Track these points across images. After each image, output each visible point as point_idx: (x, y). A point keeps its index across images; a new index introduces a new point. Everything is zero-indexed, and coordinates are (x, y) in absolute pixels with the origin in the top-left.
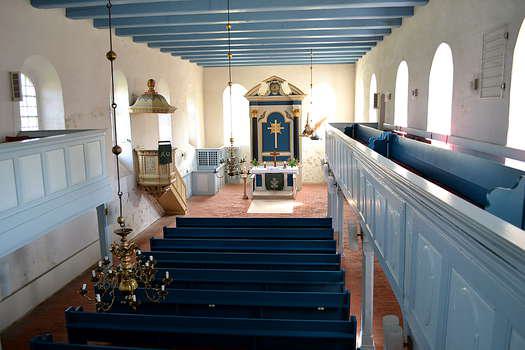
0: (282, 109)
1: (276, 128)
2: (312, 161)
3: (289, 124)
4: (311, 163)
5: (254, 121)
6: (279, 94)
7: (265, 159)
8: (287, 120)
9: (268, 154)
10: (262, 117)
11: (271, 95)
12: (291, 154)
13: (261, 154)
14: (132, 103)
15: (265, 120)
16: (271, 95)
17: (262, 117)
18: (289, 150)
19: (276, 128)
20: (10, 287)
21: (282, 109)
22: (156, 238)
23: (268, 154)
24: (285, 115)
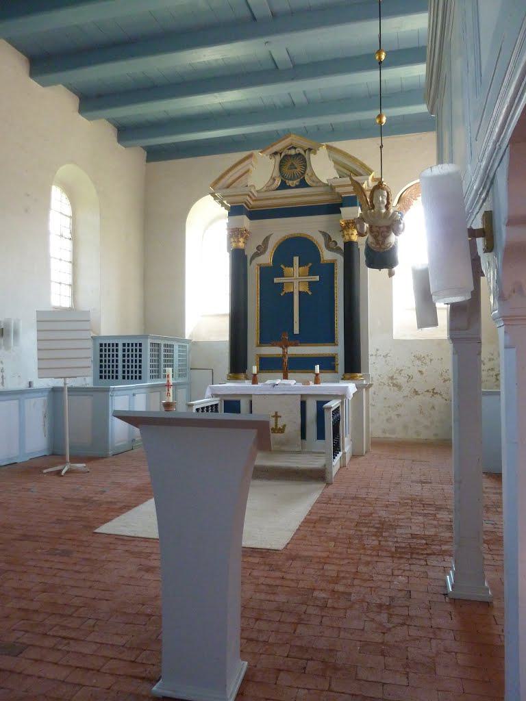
0: (311, 227)
1: (296, 279)
2: (401, 380)
3: (331, 266)
4: (399, 387)
5: (239, 261)
6: (303, 184)
7: (268, 365)
8: (327, 256)
9: (275, 351)
10: (261, 250)
11: (283, 186)
12: (337, 350)
13: (255, 350)
14: (241, 646)
15: (267, 259)
16: (283, 186)
17: (261, 250)
18: (331, 340)
19: (296, 279)
20: (503, 328)
21: (311, 227)
22: (474, 228)
23: (275, 351)
24: (320, 241)
